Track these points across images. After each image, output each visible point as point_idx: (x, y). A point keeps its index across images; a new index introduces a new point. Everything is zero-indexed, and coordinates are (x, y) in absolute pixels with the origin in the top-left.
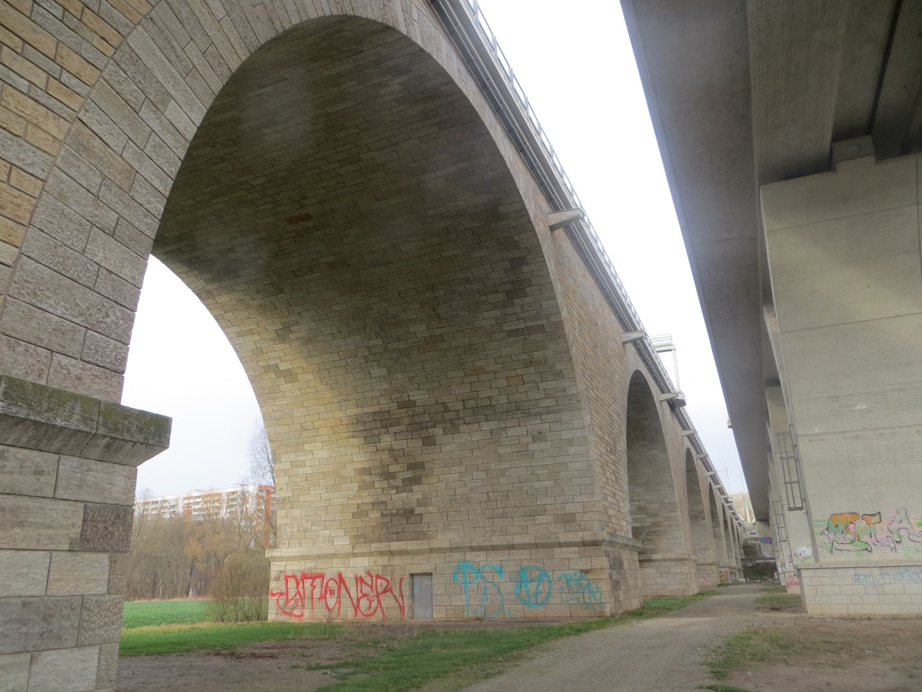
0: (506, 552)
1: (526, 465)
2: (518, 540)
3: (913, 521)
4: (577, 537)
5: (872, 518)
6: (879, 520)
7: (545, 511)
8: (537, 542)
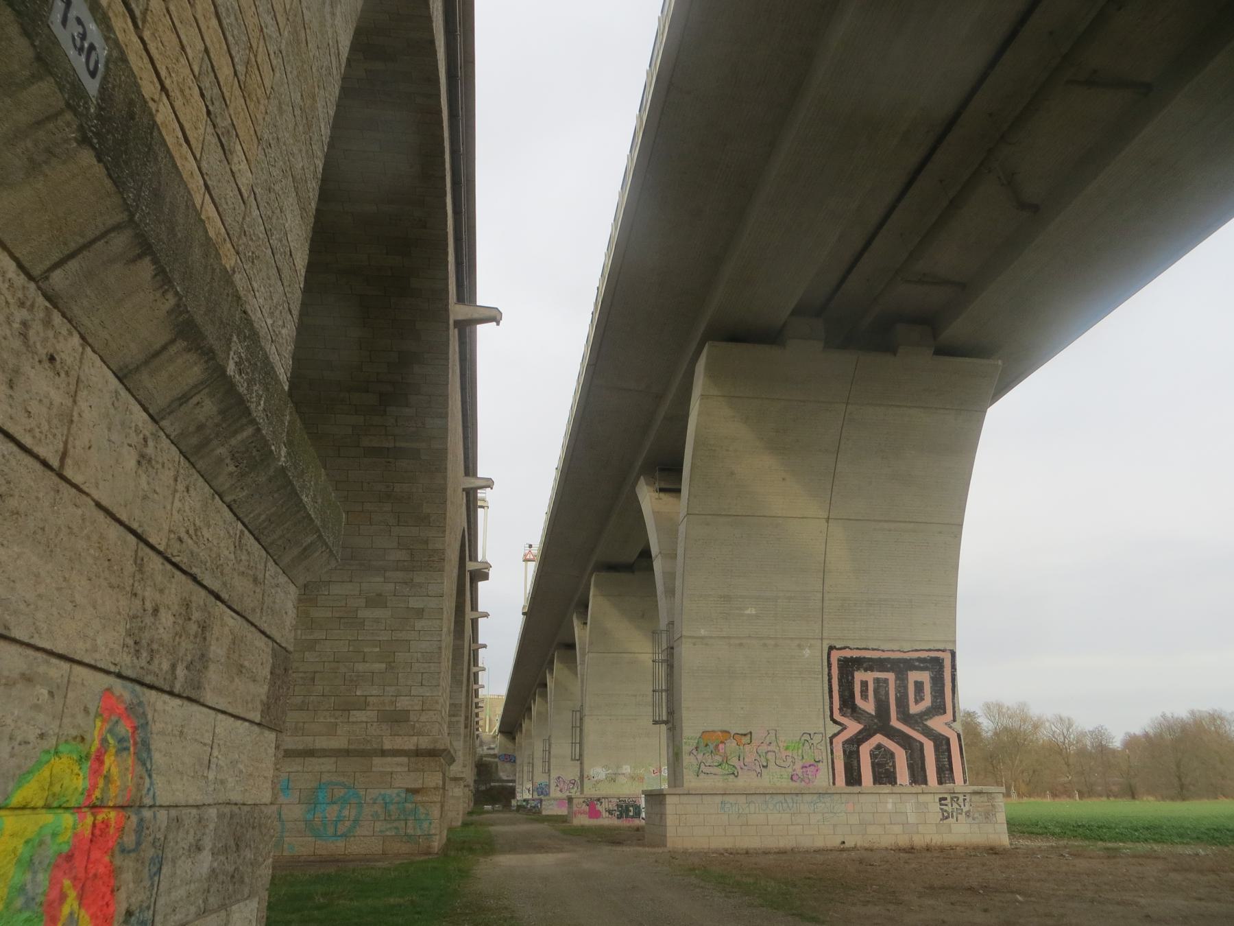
0: (298, 760)
1: (349, 638)
2: (322, 743)
3: (781, 744)
4: (409, 743)
5: (743, 738)
6: (749, 741)
7: (367, 704)
8: (351, 747)
